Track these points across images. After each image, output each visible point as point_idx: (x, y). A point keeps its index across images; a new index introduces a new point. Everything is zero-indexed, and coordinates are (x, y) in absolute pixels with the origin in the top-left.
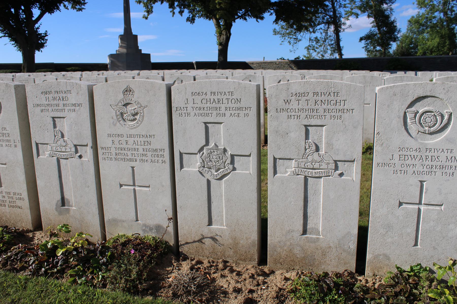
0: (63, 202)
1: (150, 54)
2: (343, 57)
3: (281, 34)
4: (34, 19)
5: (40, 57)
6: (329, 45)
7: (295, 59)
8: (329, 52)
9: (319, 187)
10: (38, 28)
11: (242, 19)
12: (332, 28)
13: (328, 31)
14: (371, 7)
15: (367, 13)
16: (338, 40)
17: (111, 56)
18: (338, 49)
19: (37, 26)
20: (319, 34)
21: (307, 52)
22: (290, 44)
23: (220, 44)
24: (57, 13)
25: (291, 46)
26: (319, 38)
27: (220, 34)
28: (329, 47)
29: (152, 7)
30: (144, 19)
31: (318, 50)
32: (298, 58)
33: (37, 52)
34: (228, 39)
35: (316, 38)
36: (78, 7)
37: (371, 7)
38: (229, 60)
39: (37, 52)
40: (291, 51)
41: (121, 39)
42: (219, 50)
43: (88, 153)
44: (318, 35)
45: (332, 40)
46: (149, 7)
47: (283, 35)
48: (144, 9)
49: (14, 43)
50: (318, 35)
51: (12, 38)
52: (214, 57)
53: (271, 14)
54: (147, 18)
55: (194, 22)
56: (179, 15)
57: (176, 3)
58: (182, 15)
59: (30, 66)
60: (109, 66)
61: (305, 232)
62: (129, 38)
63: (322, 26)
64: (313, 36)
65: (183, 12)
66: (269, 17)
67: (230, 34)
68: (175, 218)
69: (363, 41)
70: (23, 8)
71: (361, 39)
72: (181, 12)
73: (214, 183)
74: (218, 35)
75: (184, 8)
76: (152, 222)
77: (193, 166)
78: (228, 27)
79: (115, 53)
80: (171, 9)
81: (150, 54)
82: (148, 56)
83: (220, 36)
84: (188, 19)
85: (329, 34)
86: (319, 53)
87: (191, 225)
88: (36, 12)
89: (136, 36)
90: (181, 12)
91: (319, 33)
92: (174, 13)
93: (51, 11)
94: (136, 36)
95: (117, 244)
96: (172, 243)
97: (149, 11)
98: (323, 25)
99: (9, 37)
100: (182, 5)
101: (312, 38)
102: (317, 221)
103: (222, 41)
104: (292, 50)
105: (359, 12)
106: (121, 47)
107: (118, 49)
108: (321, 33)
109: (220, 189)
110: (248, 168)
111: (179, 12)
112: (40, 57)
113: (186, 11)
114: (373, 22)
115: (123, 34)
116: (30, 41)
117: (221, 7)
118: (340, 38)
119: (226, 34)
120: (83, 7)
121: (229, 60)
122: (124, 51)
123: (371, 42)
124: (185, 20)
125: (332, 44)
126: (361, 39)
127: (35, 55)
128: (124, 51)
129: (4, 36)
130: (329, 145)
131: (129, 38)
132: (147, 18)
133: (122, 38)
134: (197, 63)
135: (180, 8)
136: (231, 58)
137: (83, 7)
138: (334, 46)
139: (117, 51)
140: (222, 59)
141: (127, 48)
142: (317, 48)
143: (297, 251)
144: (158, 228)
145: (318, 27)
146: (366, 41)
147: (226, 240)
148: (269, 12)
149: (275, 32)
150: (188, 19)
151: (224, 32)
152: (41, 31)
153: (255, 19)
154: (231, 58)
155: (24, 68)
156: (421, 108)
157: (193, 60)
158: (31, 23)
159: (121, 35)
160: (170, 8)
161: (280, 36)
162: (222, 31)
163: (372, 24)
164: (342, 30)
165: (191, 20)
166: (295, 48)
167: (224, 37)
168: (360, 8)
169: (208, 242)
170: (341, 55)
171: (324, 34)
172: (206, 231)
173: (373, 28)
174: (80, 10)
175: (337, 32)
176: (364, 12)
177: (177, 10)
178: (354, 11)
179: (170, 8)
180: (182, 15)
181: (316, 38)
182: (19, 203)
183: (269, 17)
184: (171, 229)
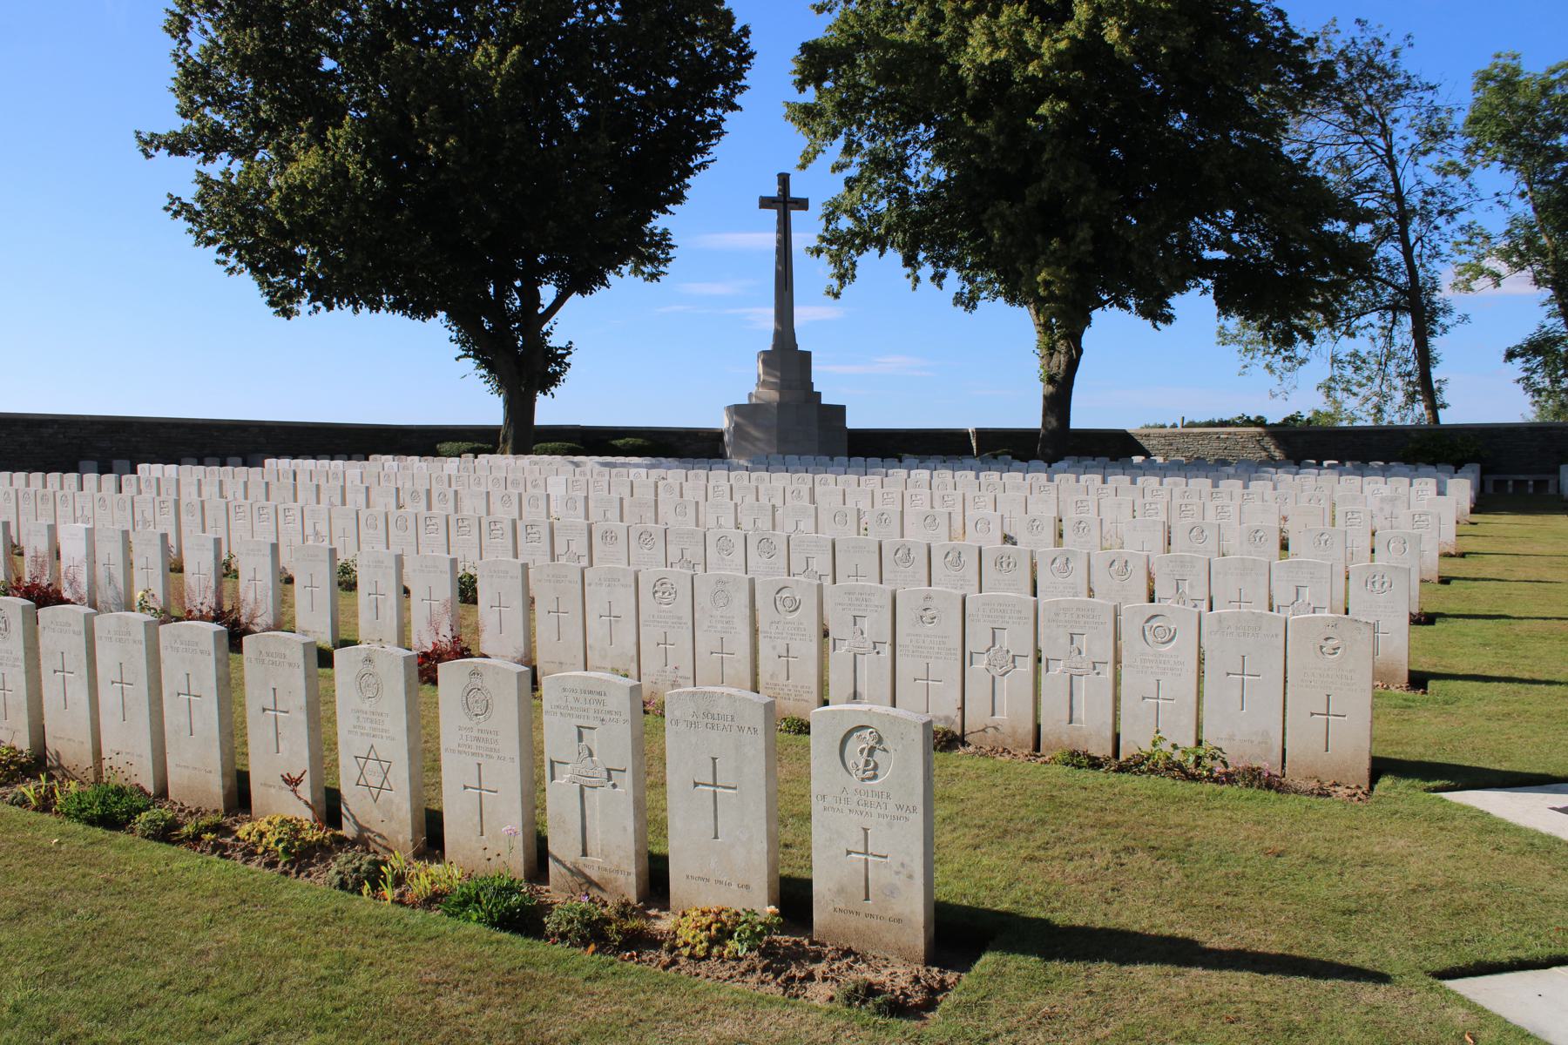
0: (1091, 590)
1: (843, 408)
2: (1446, 418)
3: (1240, 342)
4: (540, 310)
5: (549, 410)
6: (1400, 375)
7: (1286, 420)
8: (1399, 397)
9: (1082, 684)
10: (548, 334)
11: (1115, 308)
12: (1406, 321)
13: (1395, 333)
14: (1542, 252)
15: (1528, 273)
16: (1425, 359)
17: (736, 410)
18: (1425, 389)
19: (545, 328)
20: (1367, 339)
21: (1324, 399)
22: (1272, 371)
23: (1051, 380)
24: (600, 293)
25: (1275, 379)
26: (1363, 354)
27: (1051, 350)
28: (1398, 382)
29: (854, 264)
30: (831, 298)
31: (1363, 392)
32: (1293, 419)
33: (540, 396)
34: (1073, 365)
35: (1355, 355)
36: (648, 269)
37: (1542, 252)
38: (1072, 426)
39: (540, 396)
40: (1273, 396)
41: (764, 362)
42: (1045, 397)
43: (887, 650)
44: (1362, 344)
45: (1407, 361)
46: (847, 264)
47: (1248, 348)
48: (831, 269)
49: (484, 372)
50: (1362, 344)
51: (482, 361)
52: (1028, 415)
53: (1206, 291)
54: (837, 296)
55: (974, 307)
56: (933, 286)
57: (922, 256)
58: (940, 286)
59: (523, 436)
60: (726, 438)
61: (1071, 722)
62: (788, 360)
63: (1373, 317)
64: (1346, 346)
65: (943, 276)
66: (1195, 306)
67: (1080, 351)
68: (963, 709)
69: (1518, 361)
70: (518, 283)
71: (1510, 355)
72: (938, 278)
73: (998, 679)
74: (1045, 352)
75: (947, 265)
76: (941, 714)
77: (979, 665)
78: (1074, 341)
79: (746, 402)
80: (909, 270)
81: (843, 408)
82: (840, 411)
83: (1051, 355)
84: (958, 299)
85: (1398, 341)
86: (1367, 400)
87: (977, 717)
88: (548, 293)
89: (807, 356)
90: (938, 278)
91: (1367, 337)
92: (917, 279)
93: (584, 287)
94: (807, 356)
95: (1404, 135)
96: (958, 733)
97: (845, 276)
98: (1376, 314)
99: (476, 357)
100: (940, 258)
101: (1340, 357)
102: (1081, 712)
103: (1055, 370)
104: (1277, 390)
105: (1502, 267)
106: (764, 384)
107: (754, 390)
108: (1373, 339)
109: (1003, 684)
110: (1026, 666)
111: (933, 279)
112: (549, 410)
113: (952, 273)
114: (1550, 301)
115: (769, 348)
116: (523, 364)
117: (1052, 293)
118: (1433, 354)
119: (1069, 350)
120: (662, 268)
121: (1072, 426)
122: (772, 396)
123: (1545, 364)
124: (951, 302)
125: (1409, 374)
126: (1510, 355)
127: (537, 404)
128: (772, 396)
129: (466, 356)
130: (1088, 650)
131: (788, 360)
132: (837, 296)
133: (768, 359)
134: (982, 434)
135: (935, 265)
136: (1082, 417)
137: (662, 268)
138: (1413, 379)
139: (750, 395)
140: (1054, 423)
141: (783, 387)
142: (1360, 385)
143: (1064, 737)
144: (947, 719)
145: (1363, 321)
146: (1528, 361)
147: (1005, 729)
148: (1197, 286)
149: (1224, 337)
150: (958, 299)
151: (1062, 346)
152: (555, 341)
153: (1149, 322)
154: (1082, 417)
155: (505, 441)
156: (1155, 623)
157: (969, 421)
158: (534, 319)
159: (765, 352)
160: (906, 265)
161: (1237, 347)
162: (1054, 342)
163: (1550, 307)
164: (1439, 330)
165: (967, 302)
166: (1285, 385)
167: (1060, 359)
168: (1505, 255)
169: (990, 731)
170: (1433, 407)
171: (1381, 342)
172: (989, 721)
173: (1553, 320)
174: (653, 277)
175: (1421, 335)
176: (1520, 267)
177: (927, 271)
178: (1488, 263)
179: (906, 265)
180: (940, 286)
181: (1355, 355)
182: (805, 696)
183: (1195, 306)
184: (958, 720)
